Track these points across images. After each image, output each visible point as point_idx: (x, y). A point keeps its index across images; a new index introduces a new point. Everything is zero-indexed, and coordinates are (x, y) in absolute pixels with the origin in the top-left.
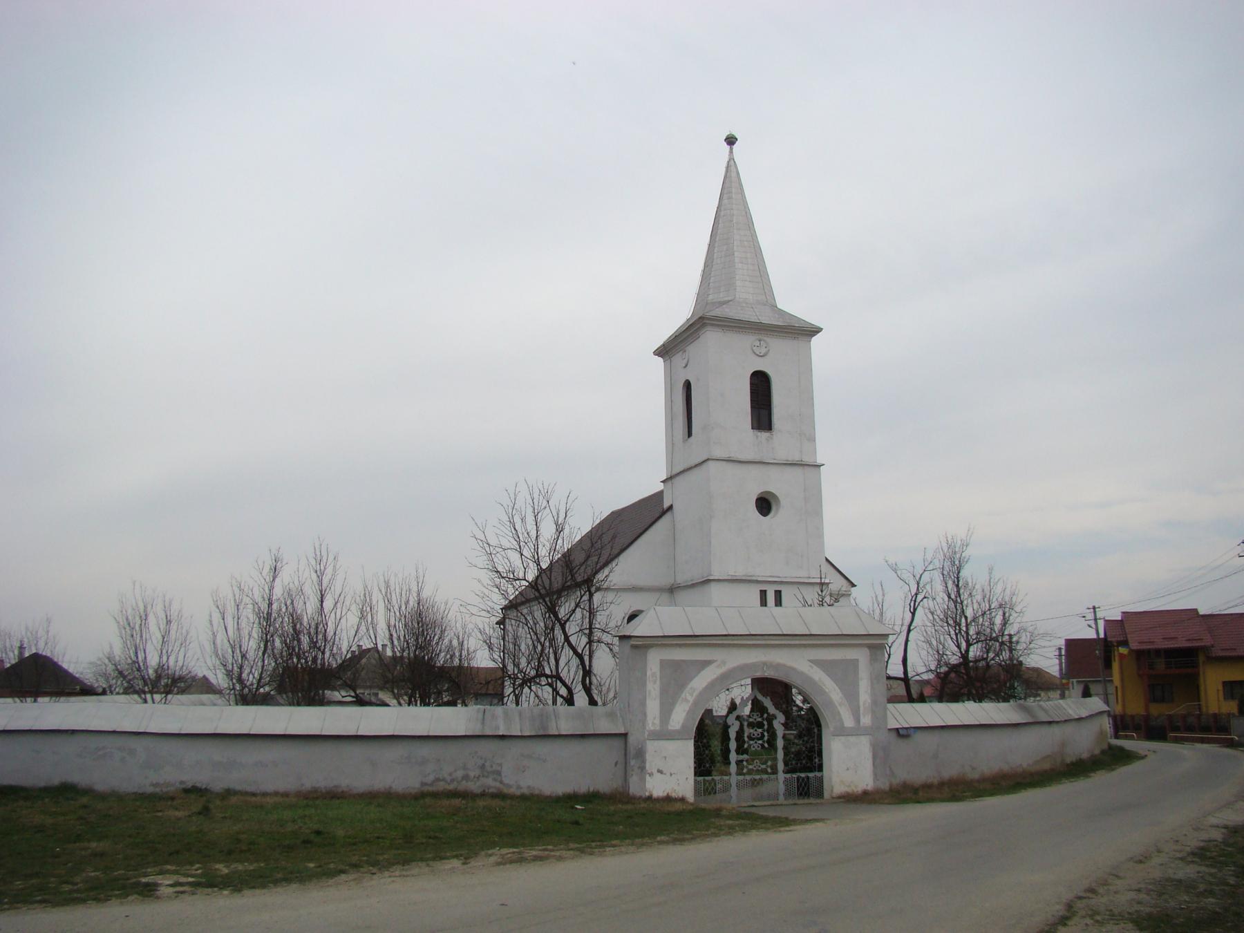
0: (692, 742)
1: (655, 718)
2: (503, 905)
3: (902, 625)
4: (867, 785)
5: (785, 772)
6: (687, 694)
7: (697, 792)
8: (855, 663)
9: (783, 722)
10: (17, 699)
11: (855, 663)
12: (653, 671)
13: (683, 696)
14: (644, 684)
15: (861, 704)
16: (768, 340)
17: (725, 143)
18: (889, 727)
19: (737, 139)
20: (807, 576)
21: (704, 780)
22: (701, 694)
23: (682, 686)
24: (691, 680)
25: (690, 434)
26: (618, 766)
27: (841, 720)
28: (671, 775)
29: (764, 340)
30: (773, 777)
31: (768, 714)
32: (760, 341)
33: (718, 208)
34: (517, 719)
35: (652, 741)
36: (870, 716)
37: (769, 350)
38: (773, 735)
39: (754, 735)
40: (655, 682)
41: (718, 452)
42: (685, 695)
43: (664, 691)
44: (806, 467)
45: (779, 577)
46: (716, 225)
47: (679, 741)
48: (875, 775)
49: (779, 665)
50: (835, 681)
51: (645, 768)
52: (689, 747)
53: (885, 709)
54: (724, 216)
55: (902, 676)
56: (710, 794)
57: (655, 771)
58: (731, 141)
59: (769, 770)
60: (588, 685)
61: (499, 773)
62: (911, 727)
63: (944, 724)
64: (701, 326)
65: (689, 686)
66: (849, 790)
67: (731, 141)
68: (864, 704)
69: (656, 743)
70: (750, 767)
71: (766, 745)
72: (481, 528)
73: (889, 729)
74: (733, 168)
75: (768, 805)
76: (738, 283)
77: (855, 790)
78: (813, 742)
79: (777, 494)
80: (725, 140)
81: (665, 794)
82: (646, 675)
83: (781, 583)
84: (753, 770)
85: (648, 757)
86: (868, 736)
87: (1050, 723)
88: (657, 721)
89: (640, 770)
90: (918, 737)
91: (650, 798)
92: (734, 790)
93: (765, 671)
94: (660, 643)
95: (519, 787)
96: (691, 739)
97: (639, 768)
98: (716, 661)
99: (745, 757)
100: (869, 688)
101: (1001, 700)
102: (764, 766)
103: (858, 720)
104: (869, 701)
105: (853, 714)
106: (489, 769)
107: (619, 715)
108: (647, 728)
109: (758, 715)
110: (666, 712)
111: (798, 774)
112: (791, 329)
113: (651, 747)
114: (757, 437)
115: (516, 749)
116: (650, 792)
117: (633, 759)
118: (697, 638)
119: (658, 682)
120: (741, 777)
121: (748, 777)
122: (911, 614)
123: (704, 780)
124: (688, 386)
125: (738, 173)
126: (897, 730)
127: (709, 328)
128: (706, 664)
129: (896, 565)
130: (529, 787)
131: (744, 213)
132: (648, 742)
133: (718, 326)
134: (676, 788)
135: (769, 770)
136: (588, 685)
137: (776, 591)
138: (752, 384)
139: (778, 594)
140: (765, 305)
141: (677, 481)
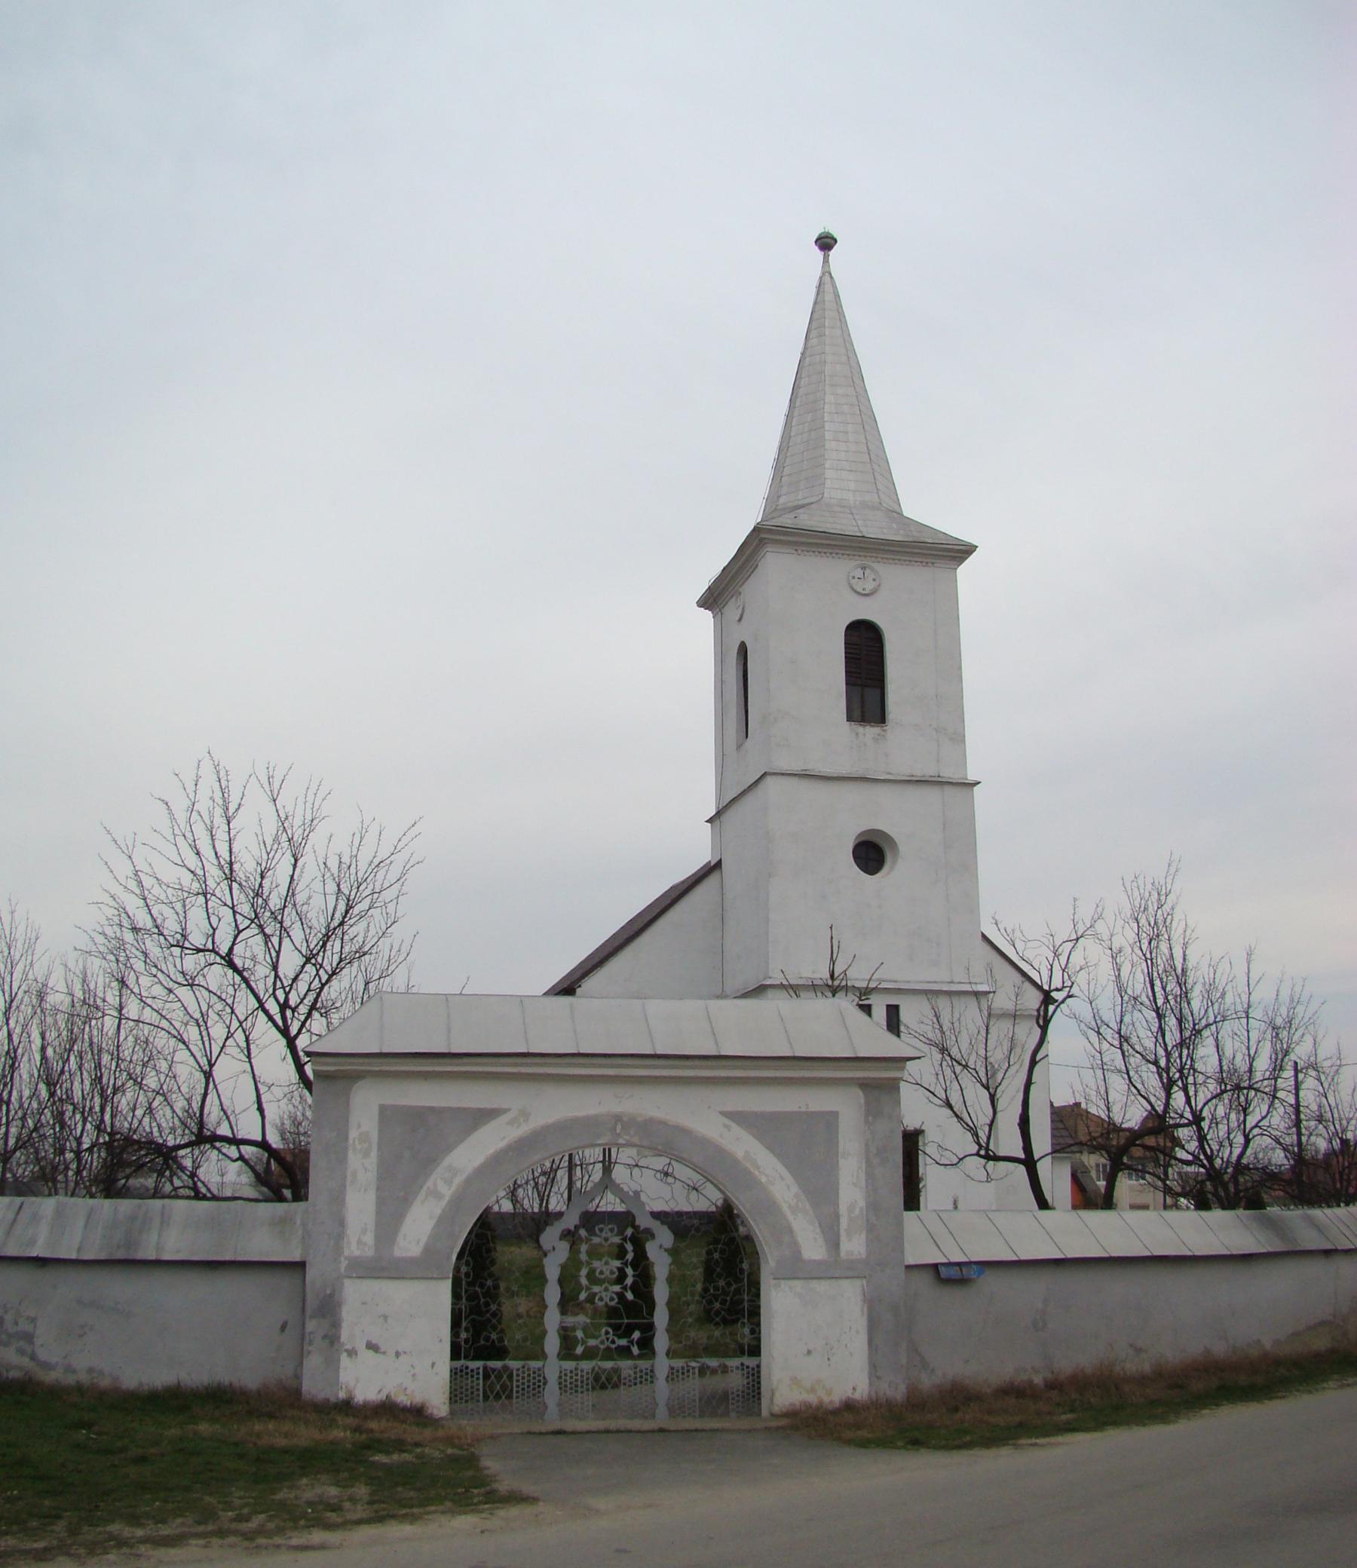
0: (445, 1289)
1: (364, 1231)
4: (854, 1389)
6: (439, 1181)
7: (456, 1395)
8: (830, 1120)
11: (830, 1120)
13: (430, 1183)
14: (342, 1160)
15: (843, 1209)
18: (911, 1260)
19: (836, 241)
20: (949, 980)
21: (485, 1368)
22: (468, 1181)
23: (428, 1163)
24: (449, 1149)
25: (747, 737)
26: (287, 1330)
27: (795, 1246)
28: (398, 1354)
29: (872, 569)
30: (644, 1364)
31: (636, 1227)
32: (864, 568)
33: (802, 354)
34: (81, 1222)
36: (863, 1236)
37: (879, 585)
38: (645, 1279)
39: (601, 1273)
40: (366, 1154)
41: (783, 763)
42: (435, 1185)
43: (386, 1173)
44: (948, 789)
45: (896, 982)
48: (873, 1367)
51: (339, 1338)
52: (440, 1297)
53: (900, 1224)
54: (809, 365)
55: (260, 1139)
56: (498, 1397)
57: (361, 1346)
58: (826, 243)
59: (635, 1350)
60: (272, 1160)
61: (29, 1338)
62: (970, 1263)
64: (758, 545)
65: (447, 1161)
66: (812, 1399)
67: (826, 243)
68: (850, 1210)
71: (630, 1296)
72: (126, 851)
73: (908, 1267)
74: (828, 287)
76: (829, 474)
77: (826, 1399)
78: (738, 1291)
80: (816, 242)
81: (382, 1396)
83: (899, 991)
84: (597, 1347)
86: (858, 1282)
88: (369, 1238)
90: (991, 1282)
91: (347, 1406)
92: (551, 1394)
93: (619, 1135)
95: (69, 1369)
96: (449, 1278)
98: (509, 1110)
99: (582, 1319)
100: (863, 1176)
101: (1342, 1205)
102: (623, 1342)
103: (834, 1244)
104: (862, 1203)
106: (12, 1329)
107: (299, 1222)
108: (346, 1253)
109: (611, 1230)
110: (389, 1218)
113: (354, 1292)
115: (67, 1288)
117: (311, 1317)
118: (460, 1061)
119: (374, 1154)
120: (569, 1365)
121: (586, 1365)
122: (1039, 1031)
124: (743, 651)
125: (837, 296)
126: (935, 1267)
127: (769, 548)
128: (485, 1116)
130: (90, 1370)
131: (844, 359)
132: (347, 1282)
133: (796, 543)
136: (272, 1160)
141: (725, 818)
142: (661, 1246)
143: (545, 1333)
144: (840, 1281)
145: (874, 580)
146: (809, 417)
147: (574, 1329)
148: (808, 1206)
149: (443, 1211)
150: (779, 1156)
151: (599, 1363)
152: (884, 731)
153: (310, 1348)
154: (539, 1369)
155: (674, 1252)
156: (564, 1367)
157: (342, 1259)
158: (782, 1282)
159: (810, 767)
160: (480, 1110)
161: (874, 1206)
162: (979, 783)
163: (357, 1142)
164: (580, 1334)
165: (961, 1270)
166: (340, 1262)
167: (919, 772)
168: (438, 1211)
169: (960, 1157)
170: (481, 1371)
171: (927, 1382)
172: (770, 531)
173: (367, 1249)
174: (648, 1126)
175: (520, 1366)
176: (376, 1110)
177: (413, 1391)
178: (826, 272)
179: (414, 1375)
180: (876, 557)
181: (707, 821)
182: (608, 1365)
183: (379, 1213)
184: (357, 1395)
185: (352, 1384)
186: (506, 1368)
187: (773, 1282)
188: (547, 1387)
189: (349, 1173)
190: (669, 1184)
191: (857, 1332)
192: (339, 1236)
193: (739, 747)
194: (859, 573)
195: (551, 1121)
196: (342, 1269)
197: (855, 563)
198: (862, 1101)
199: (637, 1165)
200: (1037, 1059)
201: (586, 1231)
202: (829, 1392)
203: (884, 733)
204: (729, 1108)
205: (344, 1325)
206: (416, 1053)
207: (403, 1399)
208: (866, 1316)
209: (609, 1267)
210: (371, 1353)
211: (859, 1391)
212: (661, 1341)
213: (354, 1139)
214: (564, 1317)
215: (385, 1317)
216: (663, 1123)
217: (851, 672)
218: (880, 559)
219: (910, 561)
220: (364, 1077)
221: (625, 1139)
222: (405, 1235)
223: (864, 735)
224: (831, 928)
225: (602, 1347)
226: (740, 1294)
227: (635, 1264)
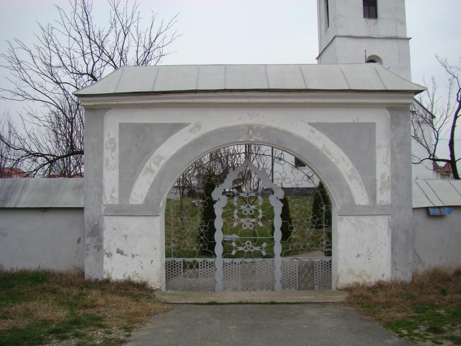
2: (382, 243)
4: (383, 275)
6: (152, 164)
8: (371, 127)
9: (282, 197)
11: (371, 127)
12: (111, 137)
13: (147, 165)
14: (101, 153)
15: (378, 177)
18: (415, 206)
21: (184, 262)
22: (168, 163)
24: (158, 146)
25: (328, 27)
28: (133, 256)
35: (111, 217)
36: (389, 192)
39: (245, 212)
40: (113, 150)
41: (341, 33)
42: (150, 165)
47: (142, 218)
48: (394, 263)
49: (269, 128)
50: (342, 146)
57: (114, 251)
65: (155, 154)
69: (115, 220)
73: (414, 209)
77: (368, 281)
84: (243, 252)
85: (107, 235)
86: (386, 217)
88: (116, 195)
89: (96, 249)
94: (115, 103)
97: (95, 247)
98: (190, 124)
99: (235, 237)
100: (389, 158)
102: (257, 249)
103: (373, 197)
104: (389, 174)
105: (366, 188)
108: (104, 202)
114: (367, 22)
116: (108, 275)
117: (88, 237)
119: (117, 150)
120: (228, 260)
123: (184, 262)
126: (427, 209)
128: (177, 127)
129: (446, 60)
132: (106, 218)
134: (139, 271)
135: (264, 253)
142: (277, 198)
143: (215, 244)
144: (376, 217)
147: (231, 242)
148: (358, 175)
149: (155, 179)
150: (341, 147)
151: (244, 259)
152: (377, 21)
153: (88, 252)
154: (212, 263)
156: (226, 261)
157: (102, 206)
158: (344, 217)
159: (351, 34)
160: (174, 124)
162: (411, 38)
163: (108, 144)
164: (234, 244)
165: (440, 211)
166: (101, 207)
167: (389, 35)
168: (152, 180)
169: (422, 160)
170: (182, 263)
171: (421, 270)
173: (115, 200)
174: (267, 131)
175: (202, 261)
176: (117, 126)
177: (142, 275)
179: (142, 267)
181: (316, 59)
183: (120, 181)
184: (113, 277)
185: (110, 271)
186: (195, 262)
187: (339, 217)
188: (216, 272)
189: (104, 160)
190: (281, 164)
191: (385, 245)
192: (100, 194)
193: (326, 31)
195: (213, 129)
196: (103, 211)
198: (389, 117)
199: (264, 155)
200: (458, 115)
201: (84, 170)
202: (369, 277)
203: (377, 22)
205: (105, 240)
206: (134, 92)
207: (136, 279)
208: (390, 236)
209: (249, 209)
211: (385, 276)
213: (107, 142)
214: (225, 235)
215: (126, 236)
216: (277, 130)
217: (364, 1)
220: (110, 109)
221: (255, 139)
222: (135, 193)
223: (370, 22)
224: (365, 51)
225: (246, 251)
226: (321, 223)
227: (263, 208)
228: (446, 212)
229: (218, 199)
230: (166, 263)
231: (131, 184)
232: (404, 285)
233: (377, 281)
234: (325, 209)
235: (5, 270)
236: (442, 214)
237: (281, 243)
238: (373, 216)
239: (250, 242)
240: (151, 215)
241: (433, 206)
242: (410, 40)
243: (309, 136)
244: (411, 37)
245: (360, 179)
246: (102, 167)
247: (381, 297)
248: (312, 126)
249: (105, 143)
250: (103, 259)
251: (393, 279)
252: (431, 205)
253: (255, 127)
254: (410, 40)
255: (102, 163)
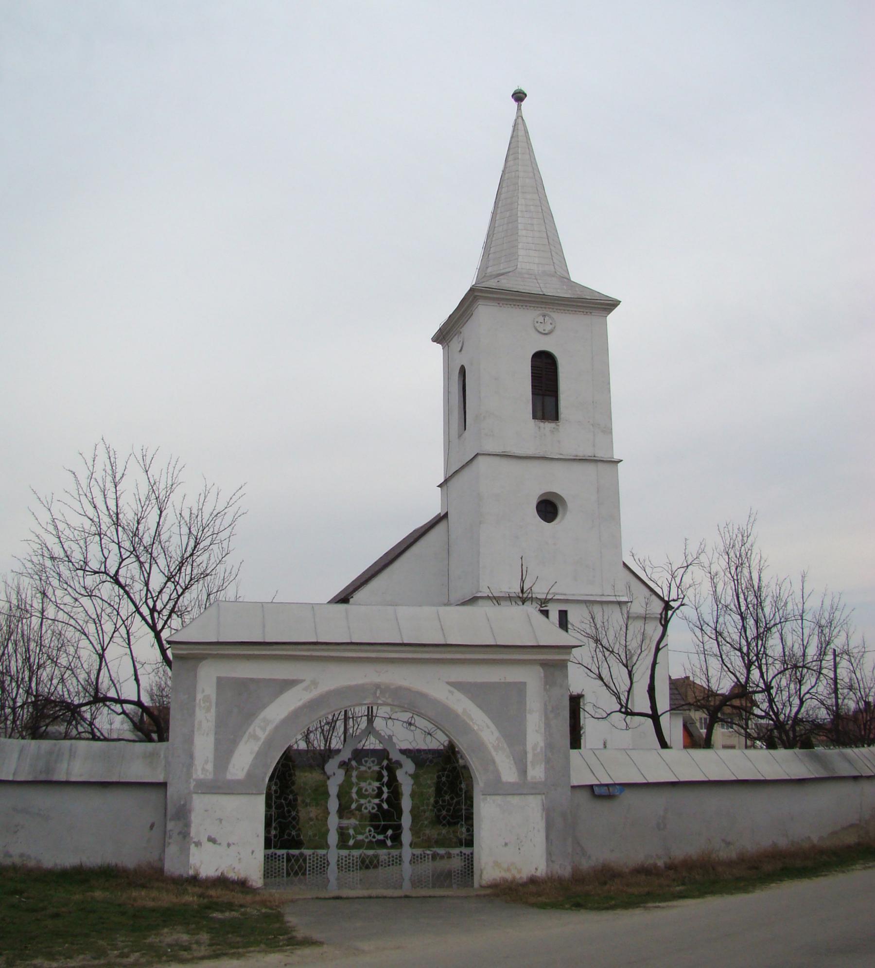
1: (206, 762)
3: (766, 664)
4: (536, 869)
5: (411, 845)
7: (268, 872)
8: (520, 688)
10: (582, 732)
11: (520, 688)
13: (251, 730)
14: (192, 714)
16: (555, 315)
17: (513, 100)
18: (575, 783)
19: (526, 95)
20: (601, 594)
21: (288, 854)
22: (277, 728)
23: (249, 716)
24: (265, 706)
25: (465, 429)
28: (229, 845)
29: (550, 317)
30: (395, 852)
31: (389, 760)
32: (544, 316)
35: (202, 796)
36: (543, 766)
37: (555, 328)
39: (366, 790)
40: (208, 710)
42: (254, 730)
43: (221, 723)
44: (600, 465)
45: (565, 595)
46: (499, 191)
48: (549, 854)
49: (399, 689)
54: (508, 179)
56: (296, 874)
57: (204, 839)
58: (519, 96)
59: (389, 843)
60: (145, 714)
62: (615, 785)
63: (675, 780)
66: (508, 876)
67: (519, 96)
70: (360, 837)
71: (385, 806)
72: (45, 503)
73: (573, 787)
74: (520, 127)
75: (364, 898)
76: (521, 252)
77: (518, 876)
78: (458, 803)
79: (562, 495)
80: (512, 96)
81: (218, 873)
82: (195, 700)
83: (567, 601)
85: (195, 818)
86: (539, 797)
87: (855, 778)
88: (210, 767)
91: (194, 880)
92: (332, 872)
93: (378, 698)
94: (216, 653)
100: (543, 725)
102: (381, 837)
103: (523, 772)
104: (542, 744)
105: (515, 763)
108: (194, 776)
109: (373, 762)
110: (223, 754)
111: (434, 849)
112: (583, 302)
113: (200, 804)
119: (213, 710)
120: (345, 852)
121: (356, 853)
124: (463, 371)
125: (526, 132)
126: (591, 787)
127: (481, 302)
128: (287, 685)
130: (22, 855)
132: (195, 796)
136: (145, 714)
137: (560, 611)
138: (533, 367)
139: (563, 615)
140: (553, 276)
142: (406, 773)
143: (328, 831)
144: (527, 797)
145: (551, 324)
146: (508, 214)
147: (348, 828)
148: (505, 746)
153: (170, 841)
154: (324, 855)
155: (415, 776)
157: (192, 781)
160: (284, 681)
161: (550, 746)
162: (621, 461)
164: (351, 832)
165: (609, 789)
168: (256, 749)
169: (608, 713)
170: (285, 856)
172: (481, 291)
173: (208, 774)
175: (311, 853)
176: (214, 680)
178: (519, 116)
180: (553, 309)
181: (438, 486)
182: (371, 852)
183: (216, 749)
185: (198, 865)
186: (301, 854)
187: (482, 797)
190: (412, 731)
191: (539, 831)
192: (190, 765)
193: (460, 436)
194: (541, 319)
195: (332, 688)
196: (192, 788)
197: (539, 312)
198: (542, 675)
199: (390, 718)
202: (520, 871)
203: (558, 427)
204: (452, 680)
205: (193, 825)
206: (242, 642)
207: (232, 875)
208: (544, 820)
210: (211, 844)
212: (406, 837)
214: (341, 820)
216: (408, 690)
218: (555, 310)
219: (564, 310)
221: (382, 701)
223: (544, 428)
224: (522, 558)
225: (367, 840)
227: (389, 785)
228: (616, 791)
229: (332, 774)
230: (265, 856)
231: (230, 752)
232: (560, 880)
233: (529, 876)
234: (465, 787)
235: (44, 867)
236: (611, 794)
237: (411, 829)
238: (523, 796)
239: (372, 829)
240: (254, 792)
241: (599, 783)
242: (619, 464)
243: (447, 698)
244: (622, 459)
245: (508, 750)
246: (193, 731)
247: (532, 888)
248: (451, 686)
249: (197, 701)
250: (190, 849)
251: (550, 874)
252: (597, 783)
253: (383, 687)
254: (619, 464)
255: (193, 726)
